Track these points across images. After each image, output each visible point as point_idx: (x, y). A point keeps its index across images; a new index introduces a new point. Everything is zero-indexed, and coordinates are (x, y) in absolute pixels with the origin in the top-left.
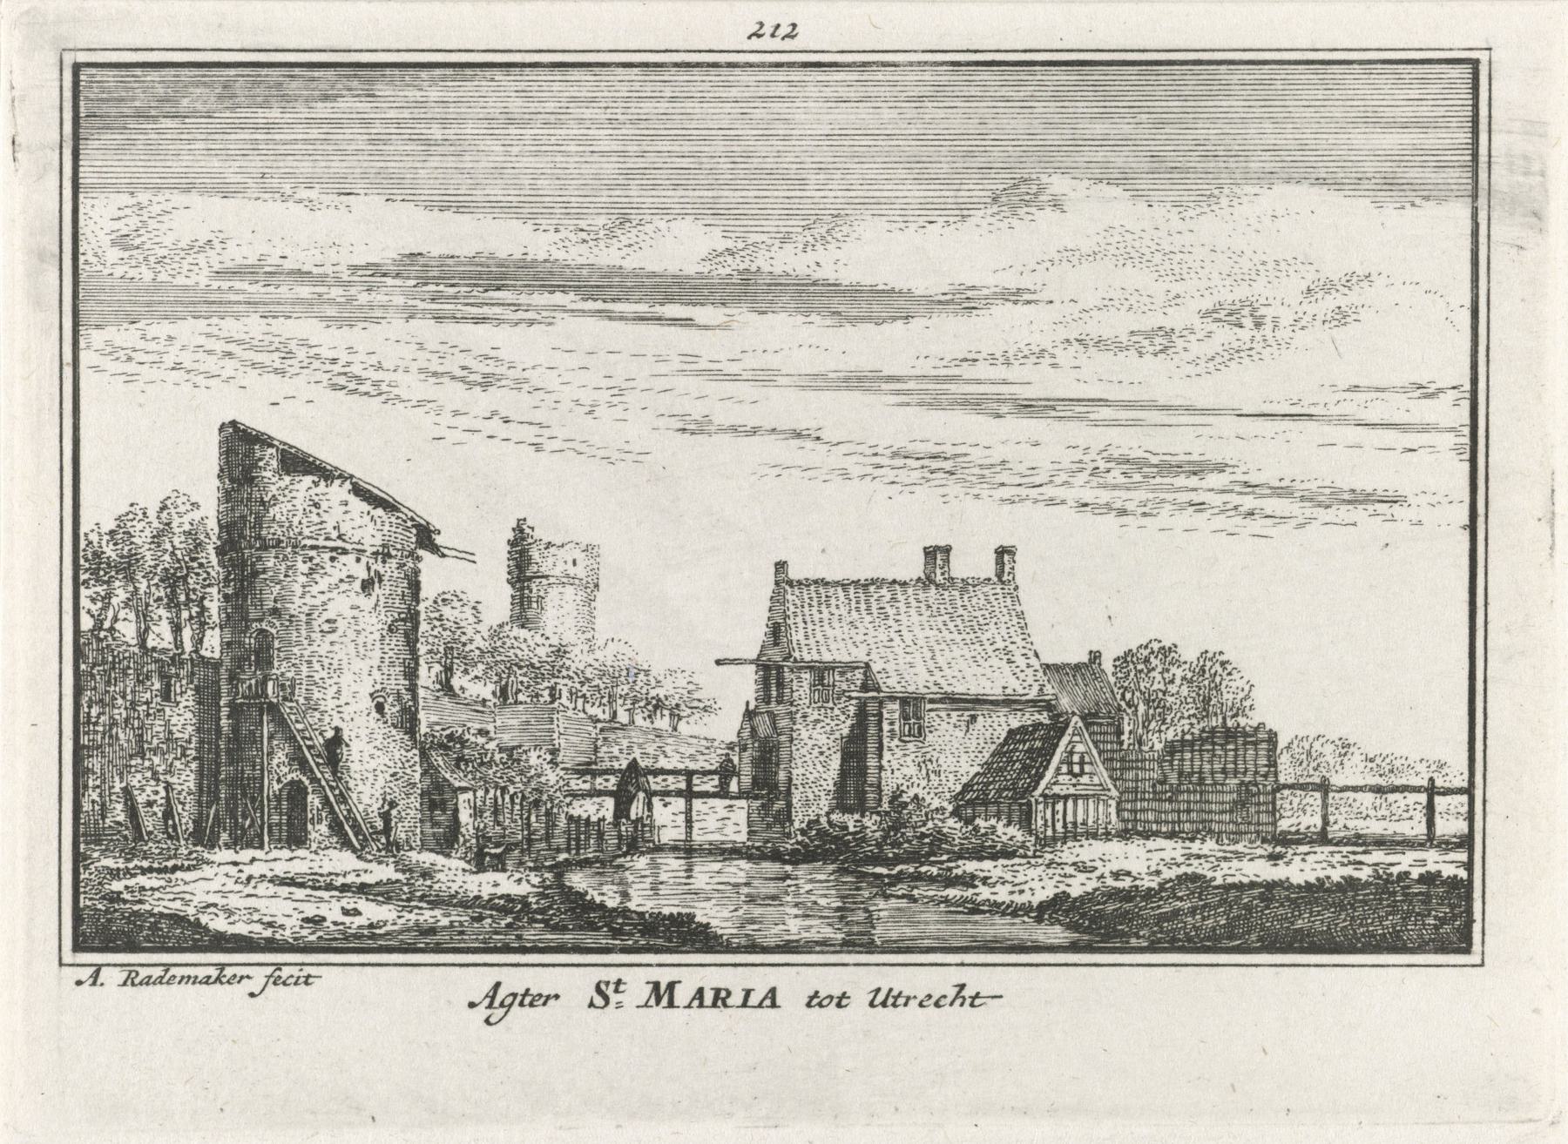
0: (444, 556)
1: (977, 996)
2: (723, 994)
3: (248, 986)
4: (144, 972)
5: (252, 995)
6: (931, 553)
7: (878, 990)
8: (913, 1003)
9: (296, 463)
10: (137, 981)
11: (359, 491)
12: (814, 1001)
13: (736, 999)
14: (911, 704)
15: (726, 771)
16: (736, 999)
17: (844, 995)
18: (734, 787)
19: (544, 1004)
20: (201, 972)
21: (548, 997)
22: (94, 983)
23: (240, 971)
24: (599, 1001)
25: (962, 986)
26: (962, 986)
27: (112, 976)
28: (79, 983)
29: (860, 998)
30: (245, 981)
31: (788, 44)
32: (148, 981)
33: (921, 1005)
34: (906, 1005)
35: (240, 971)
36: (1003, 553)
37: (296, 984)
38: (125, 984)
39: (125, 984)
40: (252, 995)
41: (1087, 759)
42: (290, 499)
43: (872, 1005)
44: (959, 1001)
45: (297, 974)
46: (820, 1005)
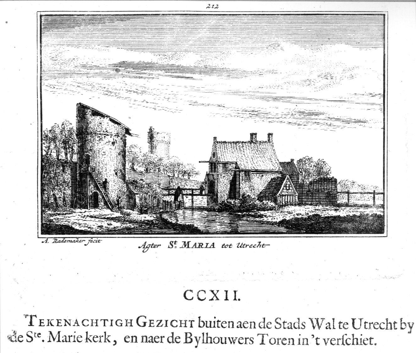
0: (132, 136)
1: (264, 245)
2: (201, 245)
3: (84, 243)
4: (59, 239)
5: (85, 245)
6: (252, 135)
7: (239, 243)
8: (248, 247)
9: (96, 113)
10: (57, 242)
11: (112, 120)
12: (224, 246)
13: (204, 245)
14: (247, 172)
15: (202, 189)
16: (204, 245)
17: (231, 245)
18: (204, 193)
19: (157, 247)
20: (73, 239)
21: (158, 245)
22: (46, 242)
23: (82, 239)
24: (171, 246)
25: (260, 242)
26: (260, 242)
27: (51, 241)
28: (43, 242)
29: (235, 246)
30: (159, 247)
31: (216, 10)
32: (60, 242)
33: (250, 247)
34: (246, 247)
35: (82, 239)
36: (270, 135)
37: (96, 242)
38: (54, 242)
39: (54, 242)
40: (85, 245)
41: (290, 186)
42: (94, 122)
43: (238, 247)
44: (259, 246)
45: (96, 240)
46: (225, 247)
